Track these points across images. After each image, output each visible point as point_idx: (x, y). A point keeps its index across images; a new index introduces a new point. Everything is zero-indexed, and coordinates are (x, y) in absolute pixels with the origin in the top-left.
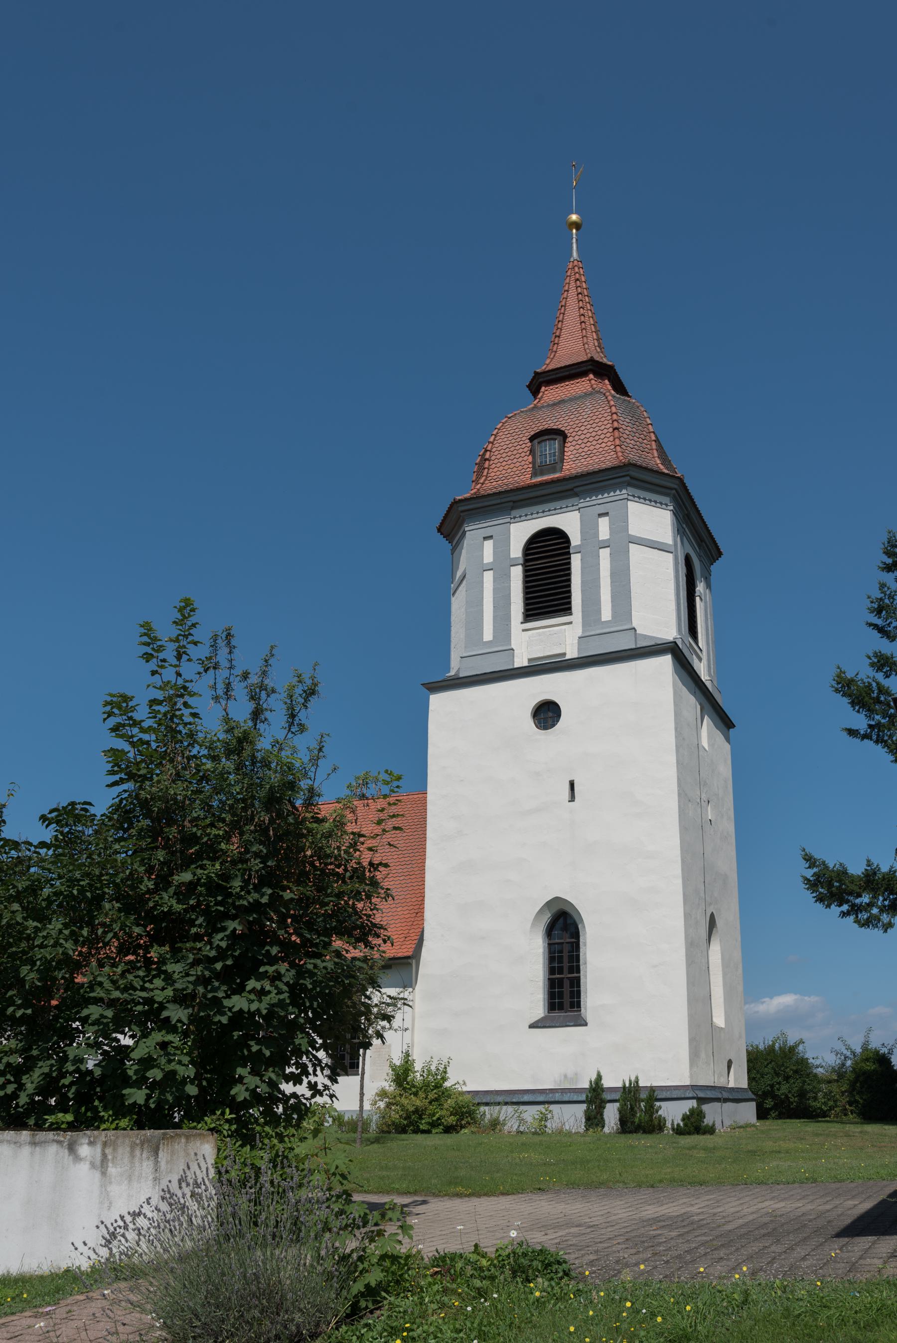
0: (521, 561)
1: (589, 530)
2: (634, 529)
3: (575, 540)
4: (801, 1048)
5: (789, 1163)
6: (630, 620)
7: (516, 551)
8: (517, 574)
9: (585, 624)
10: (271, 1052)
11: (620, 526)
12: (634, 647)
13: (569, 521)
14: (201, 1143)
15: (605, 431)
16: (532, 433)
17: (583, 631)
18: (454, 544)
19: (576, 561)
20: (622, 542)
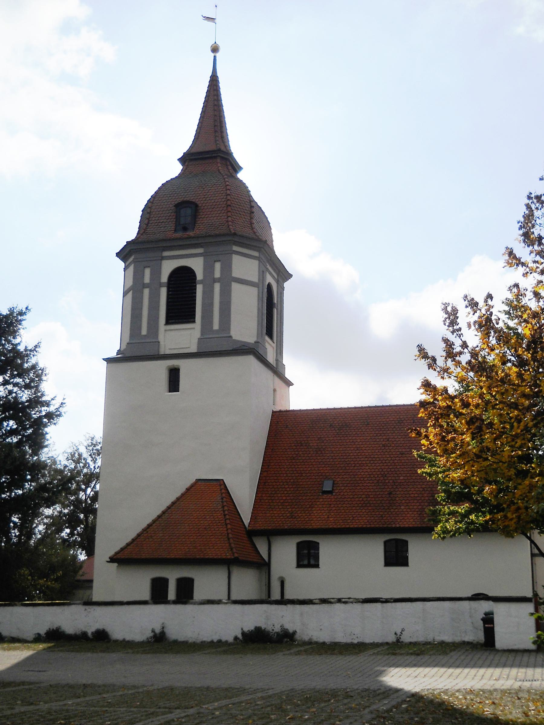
0: (166, 285)
1: (208, 269)
2: (236, 273)
3: (200, 276)
4: (244, 629)
5: (439, 526)
6: (229, 333)
7: (164, 279)
8: (164, 292)
9: (203, 332)
10: (67, 528)
11: (227, 268)
12: (215, 149)
13: (197, 264)
14: (526, 721)
15: (223, 217)
16: (176, 203)
17: (202, 335)
18: (127, 264)
19: (199, 289)
20: (227, 281)
